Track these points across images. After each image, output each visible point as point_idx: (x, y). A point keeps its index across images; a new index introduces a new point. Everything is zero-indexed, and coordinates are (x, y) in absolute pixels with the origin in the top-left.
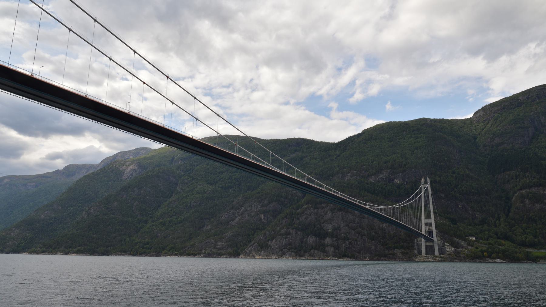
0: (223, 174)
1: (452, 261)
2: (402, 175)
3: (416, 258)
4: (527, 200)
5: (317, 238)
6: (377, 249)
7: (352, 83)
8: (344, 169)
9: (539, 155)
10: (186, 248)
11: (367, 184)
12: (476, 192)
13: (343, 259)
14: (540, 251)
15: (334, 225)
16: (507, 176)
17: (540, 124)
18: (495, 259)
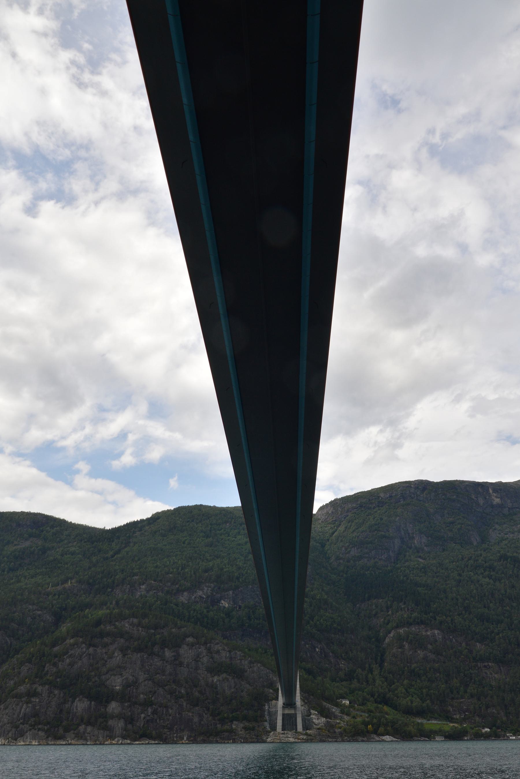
1: (323, 740)
2: (233, 593)
3: (269, 735)
4: (407, 644)
5: (93, 703)
6: (202, 723)
7: (123, 436)
8: (133, 576)
11: (177, 605)
12: (339, 627)
13: (140, 743)
14: (430, 722)
15: (127, 679)
16: (374, 607)
17: (407, 535)
18: (383, 735)
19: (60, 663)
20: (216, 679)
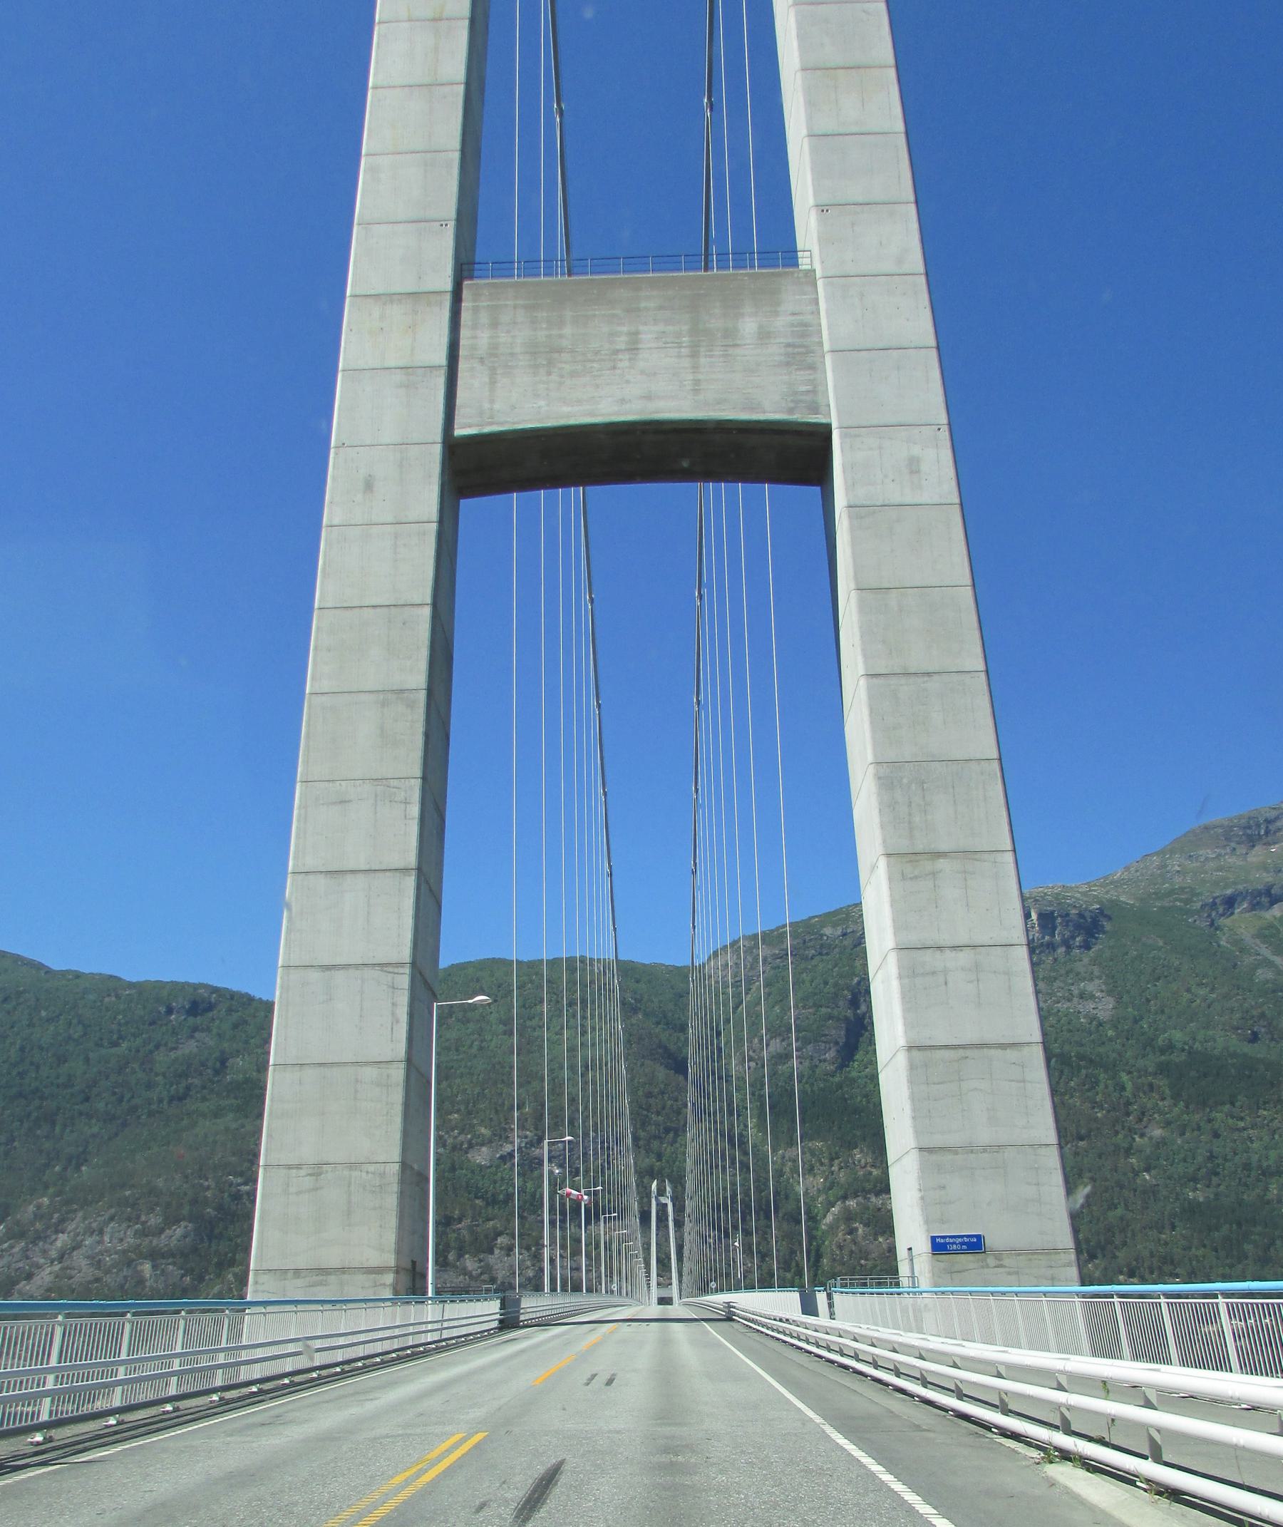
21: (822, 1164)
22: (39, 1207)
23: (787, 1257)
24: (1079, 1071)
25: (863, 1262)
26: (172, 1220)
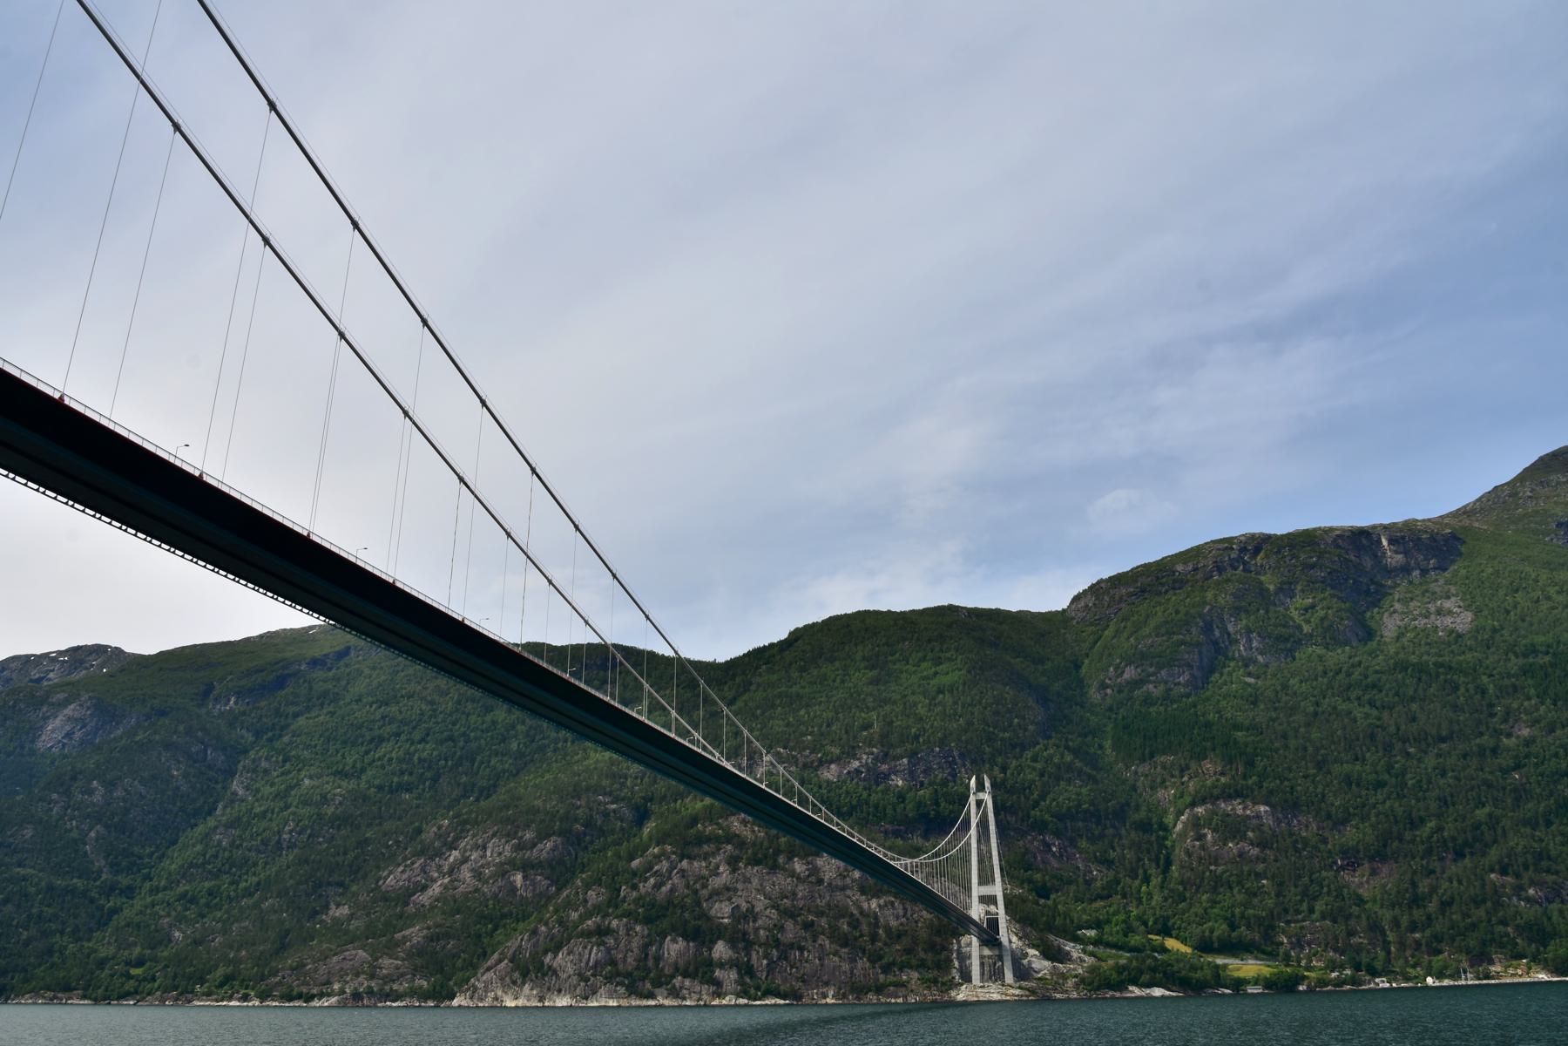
0: (384, 745)
5: (691, 944)
9: (1229, 715)
10: (275, 975)
15: (738, 907)
17: (1226, 636)
19: (641, 885)
20: (874, 904)
21: (1173, 776)
22: (440, 828)
23: (1134, 864)
24: (1437, 676)
25: (1213, 868)
26: (543, 836)
